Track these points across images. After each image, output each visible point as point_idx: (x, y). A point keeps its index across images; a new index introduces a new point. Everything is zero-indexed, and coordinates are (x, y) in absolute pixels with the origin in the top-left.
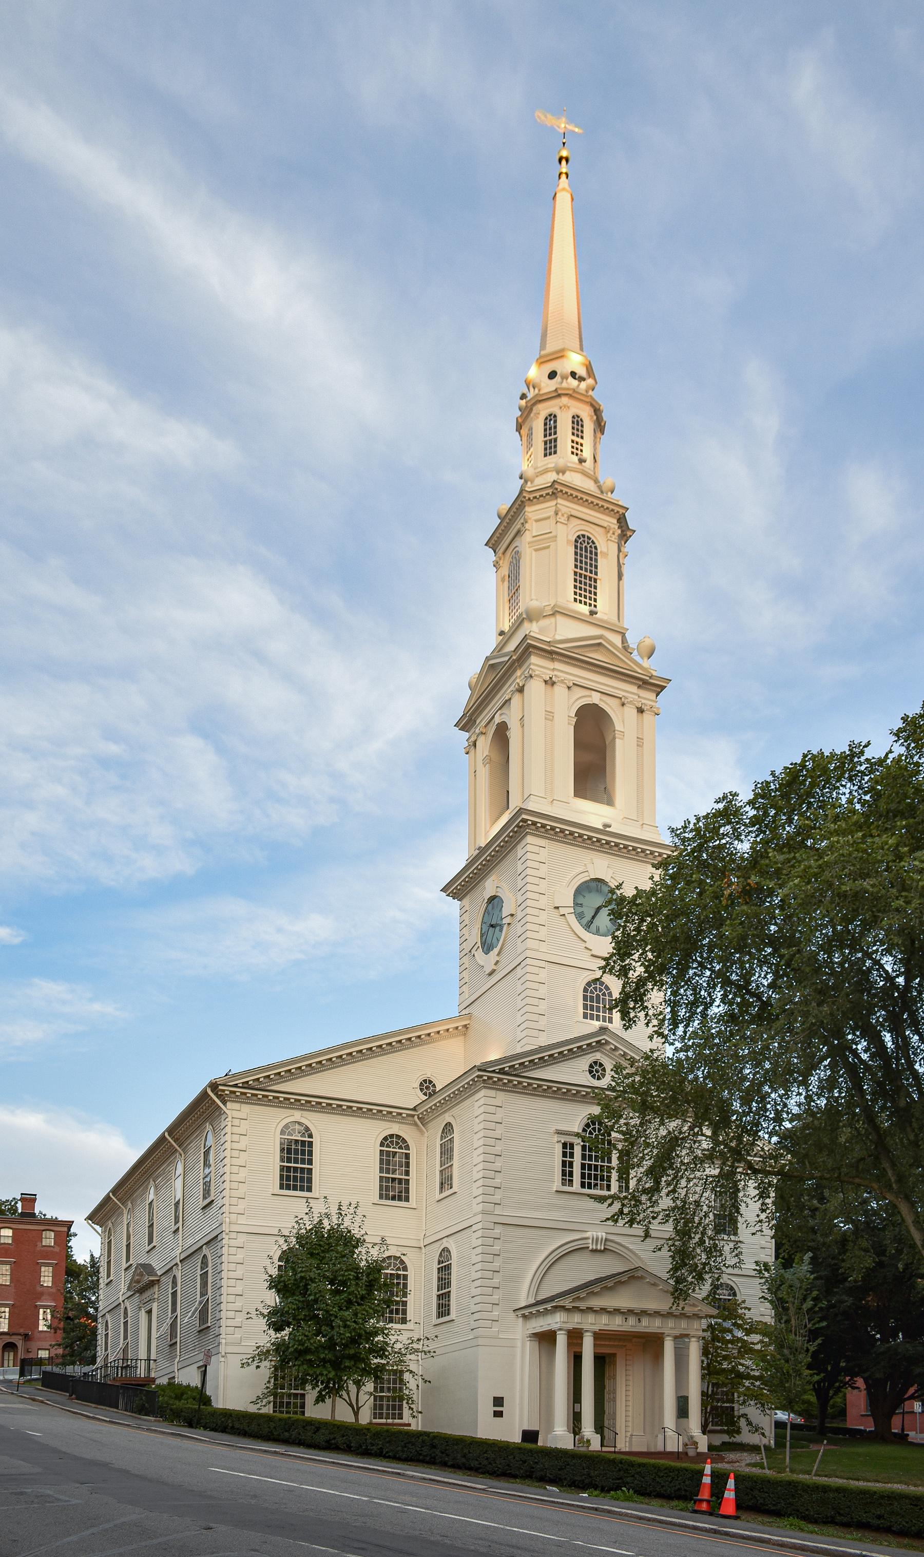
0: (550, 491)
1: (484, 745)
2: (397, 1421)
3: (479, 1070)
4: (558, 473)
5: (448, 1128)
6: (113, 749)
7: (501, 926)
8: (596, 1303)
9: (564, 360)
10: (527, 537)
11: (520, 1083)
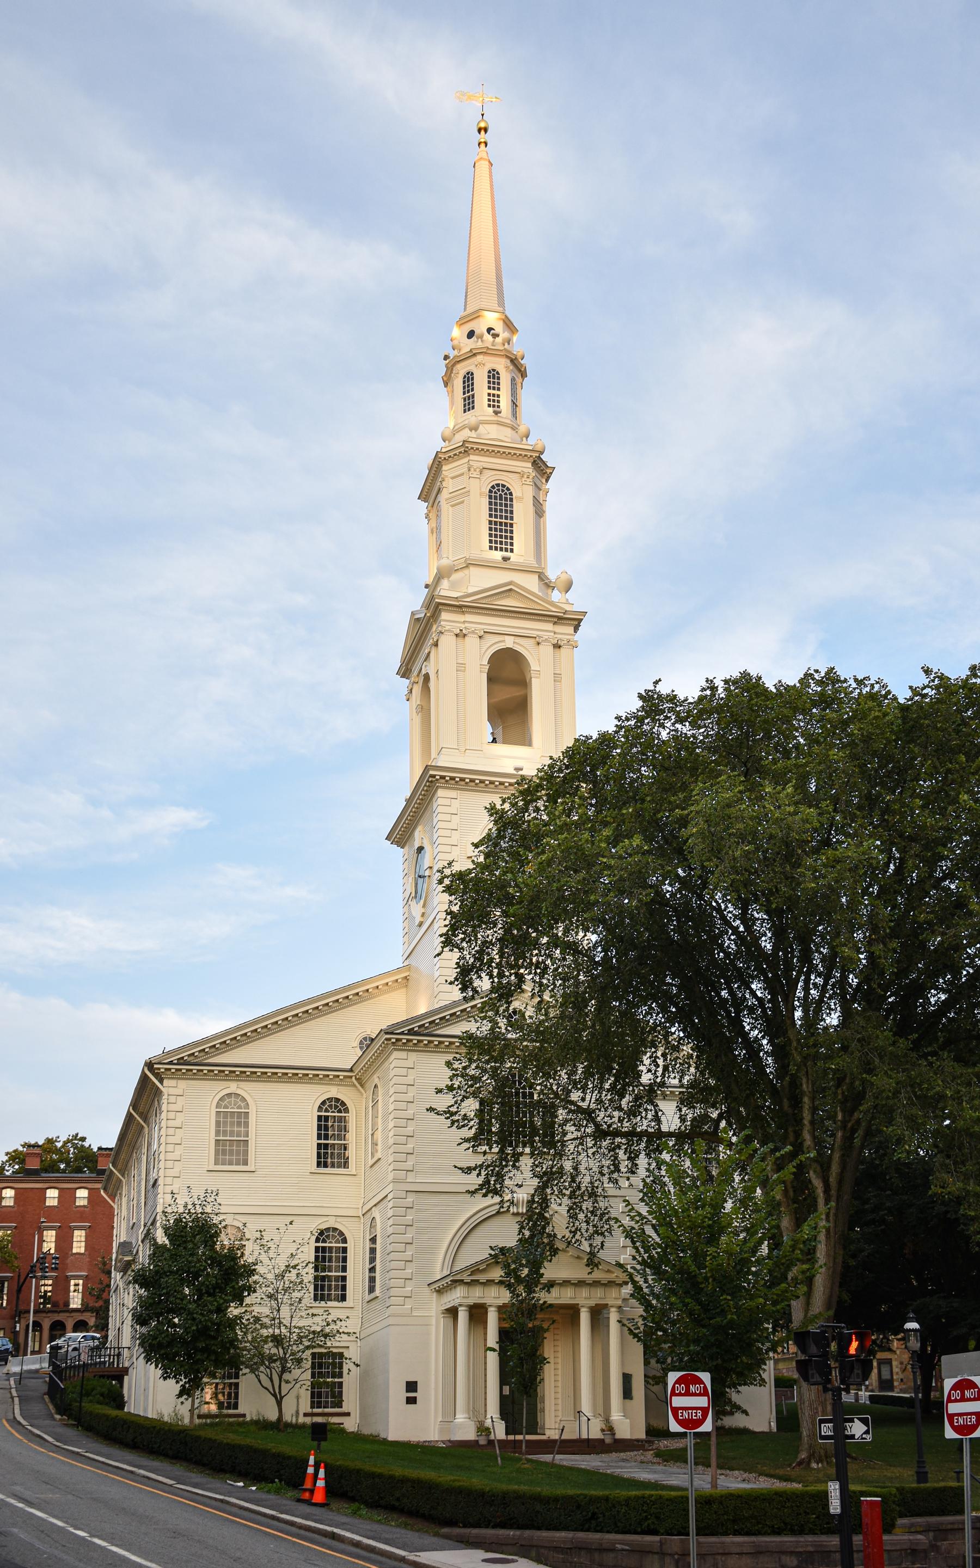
0: (462, 450)
2: (231, 1411)
3: (387, 1033)
4: (471, 430)
9: (481, 319)
10: (444, 495)
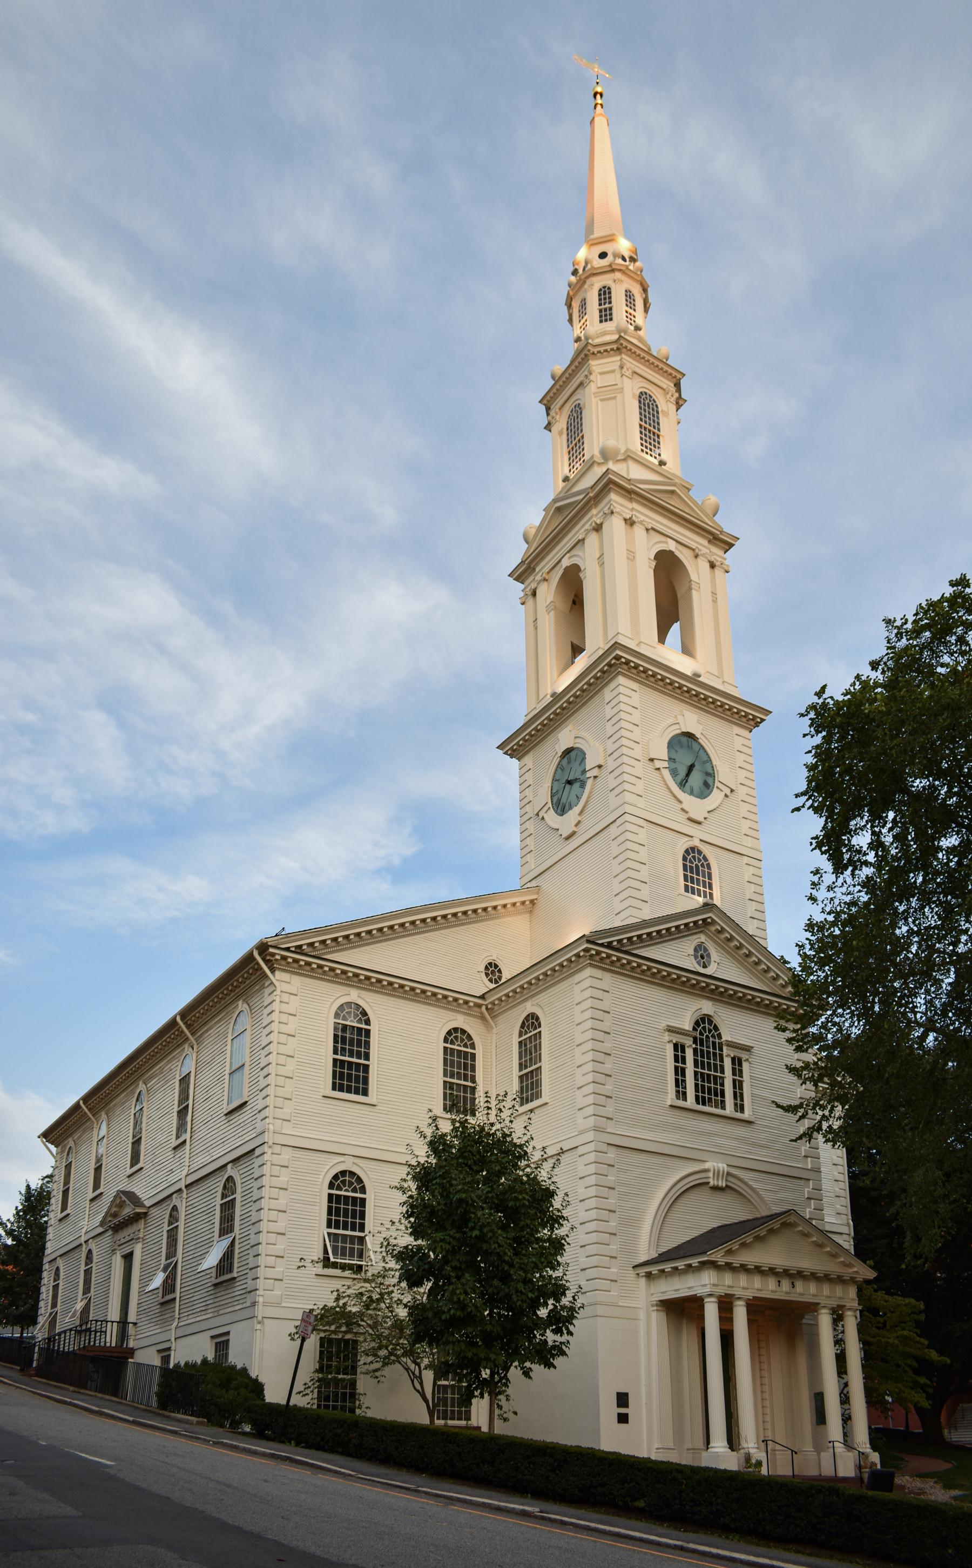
0: (615, 346)
1: (548, 593)
3: (588, 941)
5: (532, 1021)
6: (29, 717)
7: (583, 785)
8: (751, 1257)
10: (592, 388)
11: (629, 962)
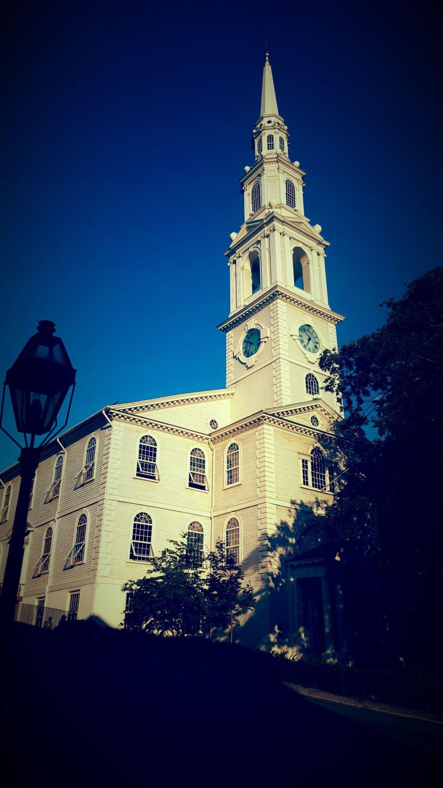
0: (276, 160)
